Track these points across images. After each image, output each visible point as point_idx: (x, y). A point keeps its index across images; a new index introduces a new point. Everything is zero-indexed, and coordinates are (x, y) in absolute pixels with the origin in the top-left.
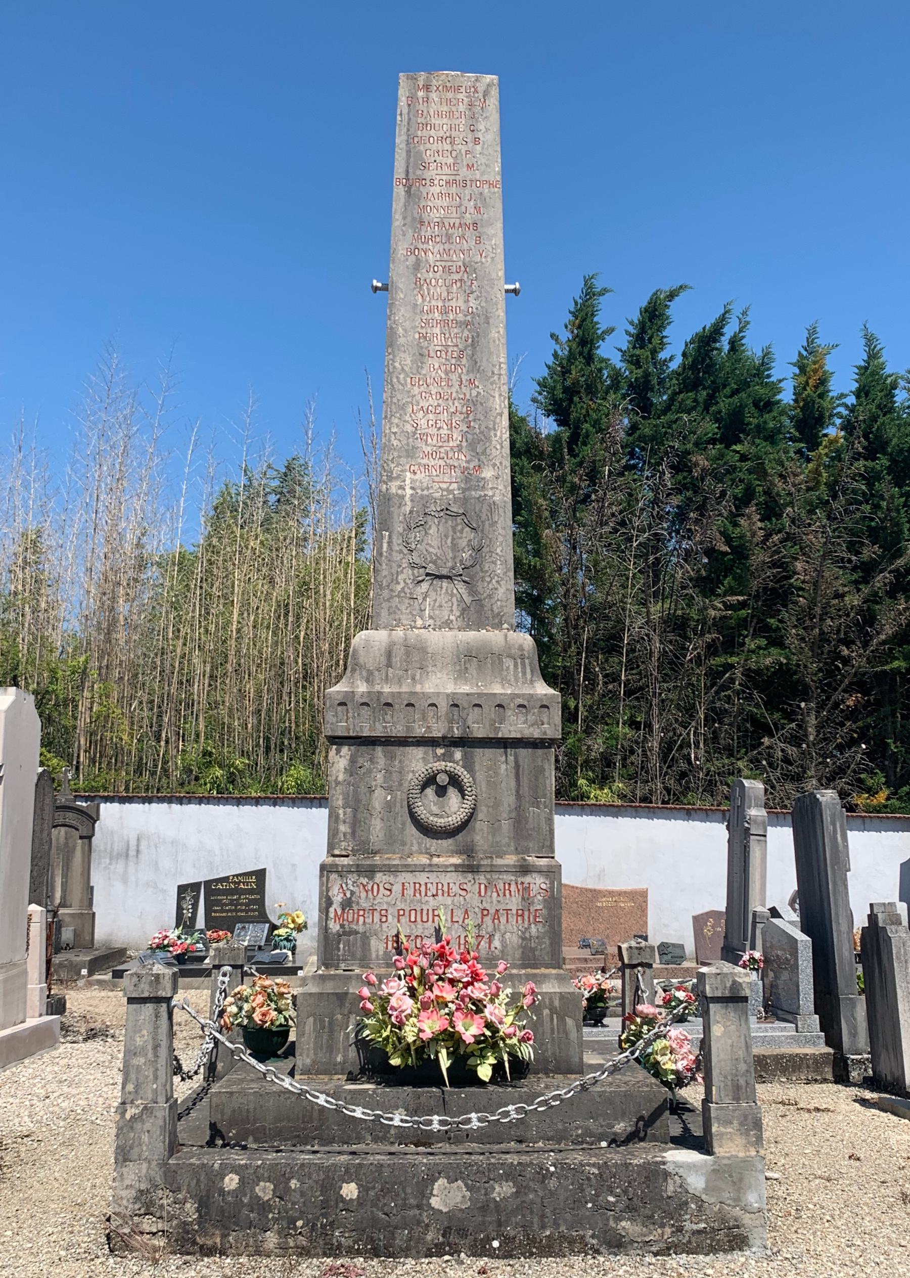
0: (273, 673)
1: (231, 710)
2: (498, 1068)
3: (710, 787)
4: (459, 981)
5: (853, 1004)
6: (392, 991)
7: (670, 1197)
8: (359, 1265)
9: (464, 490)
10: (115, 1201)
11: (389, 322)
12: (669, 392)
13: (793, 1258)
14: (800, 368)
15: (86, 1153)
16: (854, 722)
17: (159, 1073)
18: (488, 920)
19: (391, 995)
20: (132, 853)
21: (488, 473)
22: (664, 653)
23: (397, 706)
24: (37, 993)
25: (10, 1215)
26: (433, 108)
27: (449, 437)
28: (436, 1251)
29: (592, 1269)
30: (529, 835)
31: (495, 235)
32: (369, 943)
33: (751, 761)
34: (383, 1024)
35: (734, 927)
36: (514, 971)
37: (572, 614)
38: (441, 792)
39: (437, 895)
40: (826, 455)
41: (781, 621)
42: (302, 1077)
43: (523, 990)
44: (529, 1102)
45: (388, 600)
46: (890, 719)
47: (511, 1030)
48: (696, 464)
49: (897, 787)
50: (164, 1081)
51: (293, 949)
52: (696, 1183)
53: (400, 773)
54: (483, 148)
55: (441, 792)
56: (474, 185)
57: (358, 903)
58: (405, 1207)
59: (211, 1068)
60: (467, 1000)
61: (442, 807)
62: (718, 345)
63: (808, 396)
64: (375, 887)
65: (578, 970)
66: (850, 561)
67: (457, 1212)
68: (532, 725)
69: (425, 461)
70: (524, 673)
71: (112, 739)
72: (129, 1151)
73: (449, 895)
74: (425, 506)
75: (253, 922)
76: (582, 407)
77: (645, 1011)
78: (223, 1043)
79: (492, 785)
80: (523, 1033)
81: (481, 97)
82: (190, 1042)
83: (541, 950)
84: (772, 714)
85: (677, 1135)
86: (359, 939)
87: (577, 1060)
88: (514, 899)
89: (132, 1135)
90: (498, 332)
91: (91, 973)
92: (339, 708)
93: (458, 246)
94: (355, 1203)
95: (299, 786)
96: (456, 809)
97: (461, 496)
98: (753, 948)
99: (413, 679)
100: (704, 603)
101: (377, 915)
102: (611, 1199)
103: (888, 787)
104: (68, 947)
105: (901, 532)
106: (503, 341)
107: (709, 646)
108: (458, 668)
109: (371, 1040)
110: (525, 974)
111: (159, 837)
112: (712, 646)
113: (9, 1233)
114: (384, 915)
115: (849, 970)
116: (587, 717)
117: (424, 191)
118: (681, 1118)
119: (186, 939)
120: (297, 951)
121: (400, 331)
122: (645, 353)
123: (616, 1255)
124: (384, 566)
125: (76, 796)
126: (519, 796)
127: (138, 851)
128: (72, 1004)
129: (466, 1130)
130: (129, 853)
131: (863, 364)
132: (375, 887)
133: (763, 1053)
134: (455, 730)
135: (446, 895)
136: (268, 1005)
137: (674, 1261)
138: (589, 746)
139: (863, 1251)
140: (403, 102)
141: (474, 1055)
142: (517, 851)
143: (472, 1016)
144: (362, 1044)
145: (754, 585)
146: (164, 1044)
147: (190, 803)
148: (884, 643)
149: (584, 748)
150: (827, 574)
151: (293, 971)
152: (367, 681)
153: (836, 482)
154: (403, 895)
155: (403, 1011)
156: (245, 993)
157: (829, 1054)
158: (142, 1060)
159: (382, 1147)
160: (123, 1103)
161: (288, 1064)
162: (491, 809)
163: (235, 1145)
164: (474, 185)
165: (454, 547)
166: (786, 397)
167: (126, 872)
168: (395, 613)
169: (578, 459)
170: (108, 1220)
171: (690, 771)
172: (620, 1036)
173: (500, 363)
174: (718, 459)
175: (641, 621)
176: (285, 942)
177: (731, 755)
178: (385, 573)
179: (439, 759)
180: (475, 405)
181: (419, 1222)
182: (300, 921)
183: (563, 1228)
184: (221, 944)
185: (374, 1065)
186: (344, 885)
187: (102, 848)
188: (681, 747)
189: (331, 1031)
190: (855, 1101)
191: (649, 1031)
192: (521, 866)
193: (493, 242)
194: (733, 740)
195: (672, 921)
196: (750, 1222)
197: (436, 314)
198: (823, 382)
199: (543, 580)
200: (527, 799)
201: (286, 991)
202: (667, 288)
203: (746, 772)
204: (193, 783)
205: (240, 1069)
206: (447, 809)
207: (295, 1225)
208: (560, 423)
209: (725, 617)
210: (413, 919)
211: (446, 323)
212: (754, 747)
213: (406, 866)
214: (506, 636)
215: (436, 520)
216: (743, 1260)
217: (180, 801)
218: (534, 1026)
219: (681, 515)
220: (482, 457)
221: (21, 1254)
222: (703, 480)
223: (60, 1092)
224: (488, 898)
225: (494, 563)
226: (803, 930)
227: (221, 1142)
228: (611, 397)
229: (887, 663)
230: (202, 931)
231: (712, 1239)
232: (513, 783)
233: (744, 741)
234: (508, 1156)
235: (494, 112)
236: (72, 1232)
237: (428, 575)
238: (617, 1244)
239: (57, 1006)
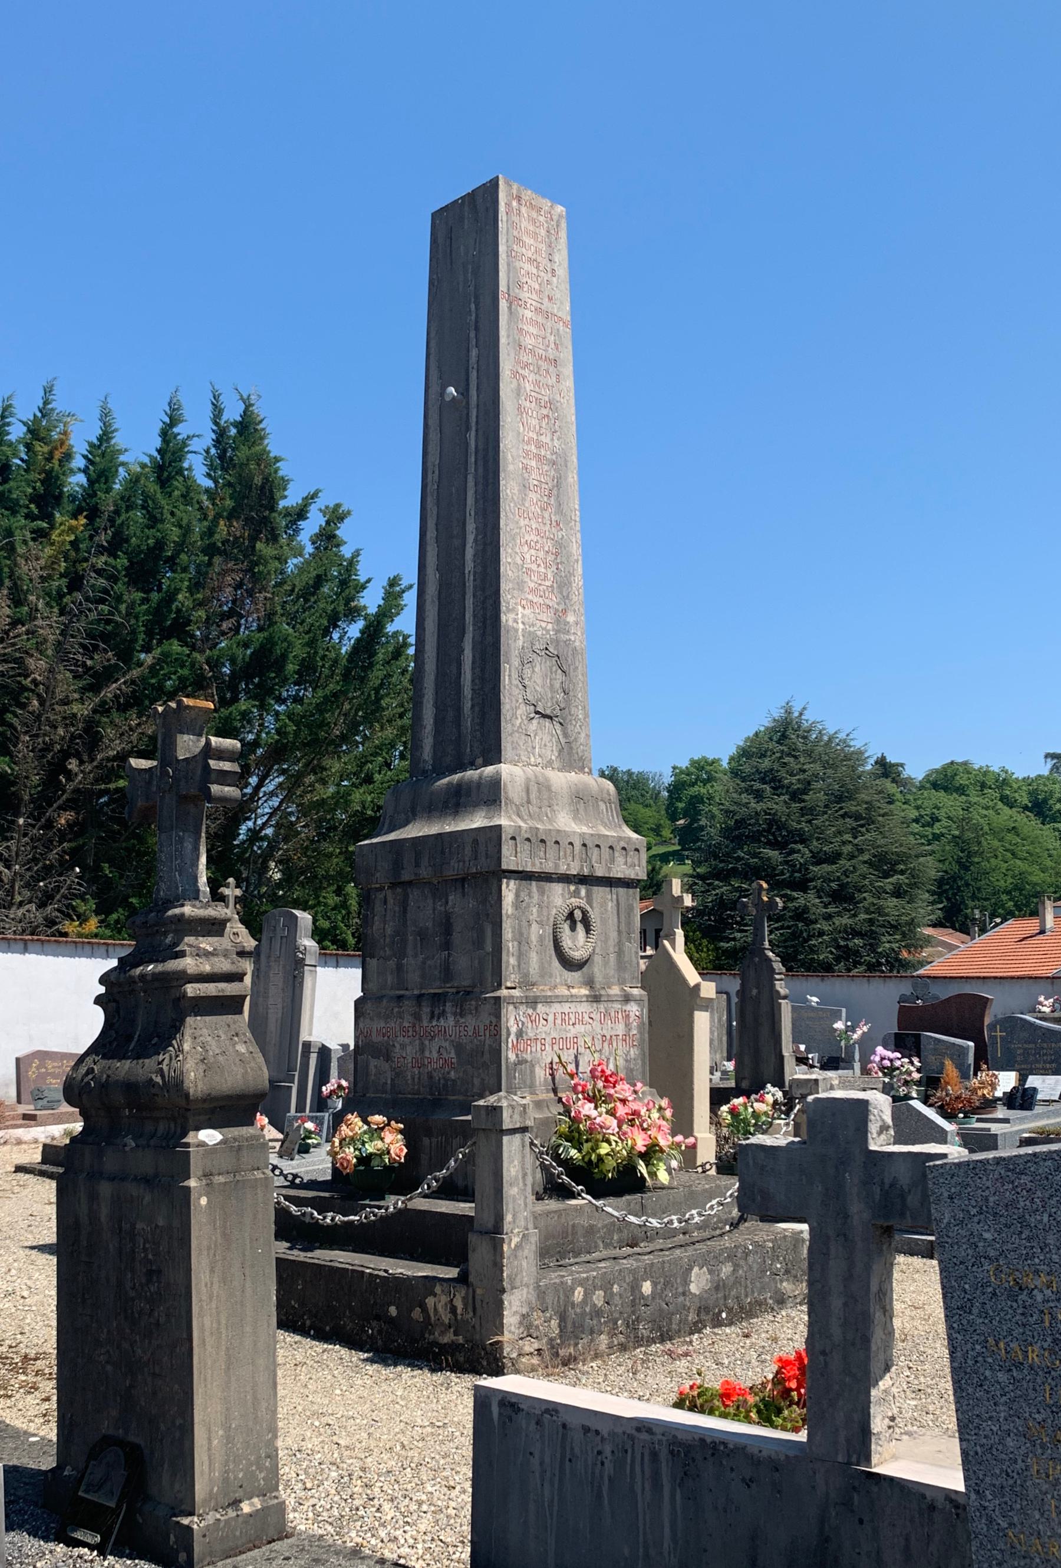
9: (557, 632)
45: (511, 735)
66: (84, 664)
69: (530, 597)
126: (619, 932)
225: (577, 707)
232: (616, 920)
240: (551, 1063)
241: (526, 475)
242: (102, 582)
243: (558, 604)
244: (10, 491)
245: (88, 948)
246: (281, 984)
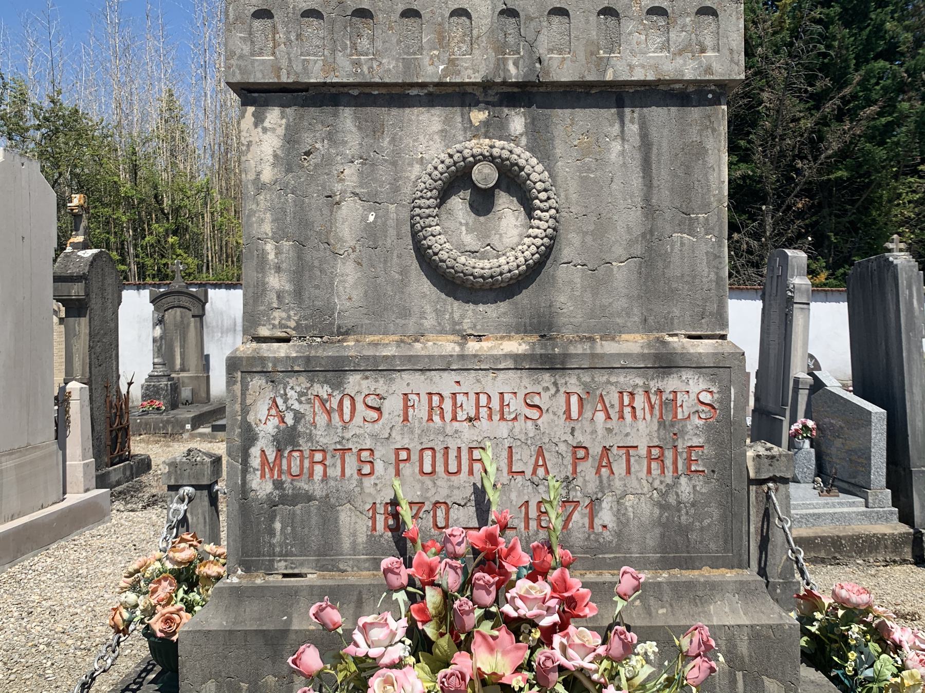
18: (587, 469)
23: (380, 17)
32: (336, 520)
38: (483, 203)
39: (477, 418)
53: (394, 164)
55: (483, 203)
57: (310, 438)
61: (484, 235)
64: (347, 403)
66: (806, 91)
68: (680, 53)
73: (502, 418)
83: (702, 529)
86: (314, 510)
88: (641, 425)
92: (257, 23)
96: (516, 240)
110: (669, 583)
114: (366, 459)
126: (650, 210)
132: (347, 403)
133: (837, 533)
135: (496, 417)
142: (645, 325)
150: (787, 102)
154: (406, 419)
157: (909, 534)
162: (589, 239)
179: (475, 132)
186: (280, 401)
187: (214, 324)
192: (657, 357)
200: (668, 215)
206: (495, 240)
210: (427, 468)
213: (410, 358)
224: (586, 424)
232: (636, 182)
242: (819, 28)
245: (822, 294)
246: (777, 321)
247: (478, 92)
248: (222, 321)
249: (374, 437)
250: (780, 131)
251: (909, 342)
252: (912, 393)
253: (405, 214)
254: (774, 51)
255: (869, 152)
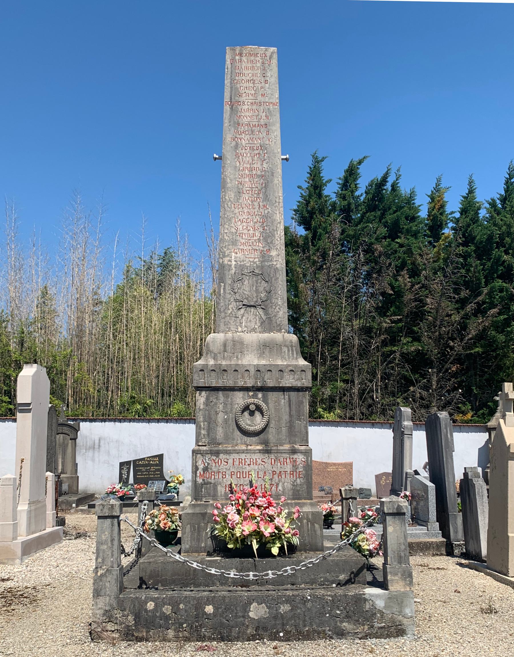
0: (164, 357)
1: (144, 376)
2: (281, 549)
3: (383, 412)
4: (262, 506)
5: (455, 517)
6: (228, 512)
7: (367, 611)
8: (214, 645)
9: (262, 262)
10: (93, 616)
11: (222, 176)
12: (361, 212)
13: (428, 640)
14: (431, 199)
15: (78, 593)
16: (456, 379)
17: (114, 553)
18: (276, 476)
19: (228, 513)
20: (96, 446)
21: (274, 253)
22: (360, 346)
23: (229, 371)
24: (51, 515)
25: (41, 623)
26: (244, 65)
27: (254, 235)
28: (252, 638)
29: (329, 646)
30: (296, 435)
31: (276, 130)
33: (404, 399)
34: (225, 528)
35: (397, 479)
36: (289, 501)
37: (315, 326)
38: (252, 414)
40: (443, 244)
41: (420, 329)
42: (185, 554)
43: (294, 510)
44: (297, 565)
45: (224, 318)
46: (474, 377)
47: (288, 530)
48: (376, 250)
49: (477, 410)
50: (116, 557)
51: (178, 493)
52: (380, 604)
54: (269, 85)
55: (252, 414)
56: (265, 104)
57: (211, 469)
58: (236, 616)
59: (139, 552)
60: (266, 515)
61: (252, 421)
62: (385, 187)
63: (435, 214)
64: (220, 461)
65: (319, 502)
66: (454, 298)
67: (262, 619)
69: (242, 247)
70: (293, 354)
71: (84, 390)
72: (100, 591)
74: (242, 270)
75: (157, 480)
76: (318, 221)
77: (354, 520)
78: (145, 538)
79: (277, 410)
80: (294, 531)
81: (268, 59)
82: (128, 539)
84: (415, 375)
85: (370, 581)
87: (320, 544)
88: (288, 466)
89: (101, 583)
90: (278, 180)
91: (77, 506)
92: (200, 372)
93: (258, 136)
94: (212, 615)
95: (179, 413)
97: (260, 265)
98: (406, 490)
99: (237, 357)
100: (381, 320)
101: (220, 475)
102: (338, 612)
103: (473, 411)
104: (66, 493)
105: (481, 283)
106: (281, 185)
107: (383, 341)
108: (260, 352)
109: (219, 536)
111: (110, 439)
112: (385, 341)
113: (41, 631)
114: (224, 475)
115: (454, 501)
116: (322, 378)
117: (240, 108)
118: (372, 573)
119: (124, 489)
120: (179, 494)
121: (228, 180)
122: (348, 193)
123: (341, 639)
124: (222, 301)
125: (68, 419)
126: (291, 416)
127: (99, 446)
128: (68, 521)
129: (266, 579)
130: (95, 447)
131: (465, 195)
132: (220, 461)
134: (259, 384)
136: (167, 519)
137: (370, 642)
138: (323, 392)
139: (462, 636)
140: (228, 62)
141: (270, 543)
142: (290, 443)
143: (269, 523)
144: (214, 538)
145: (406, 310)
146: (116, 539)
147: (125, 422)
148: (471, 339)
149: (321, 393)
150: (443, 305)
151: (178, 504)
152: (214, 359)
153: (448, 258)
155: (234, 521)
156: (156, 514)
157: (444, 542)
158: (105, 547)
159: (225, 588)
160: (96, 568)
161: (178, 547)
163: (152, 588)
164: (265, 104)
165: (257, 291)
166: (423, 214)
167: (93, 456)
168: (227, 324)
169: (316, 248)
170: (90, 625)
171: (374, 404)
172: (341, 533)
173: (279, 196)
174: (388, 247)
175: (349, 329)
176: (173, 490)
177: (394, 396)
178: (222, 304)
179: (250, 397)
180: (267, 218)
181: (243, 624)
182: (181, 479)
183: (314, 626)
184: (143, 490)
185: (220, 548)
187: (81, 444)
188: (369, 393)
189: (199, 531)
190: (457, 564)
191: (356, 530)
192: (292, 450)
193: (275, 134)
194: (395, 388)
195: (364, 478)
196: (406, 623)
197: (247, 171)
198: (442, 206)
199: (300, 309)
200: (295, 417)
201: (176, 512)
202: (356, 160)
203: (401, 404)
204: (126, 412)
205: (154, 551)
206: (255, 422)
207: (182, 626)
208: (306, 229)
209: (391, 327)
210: (238, 476)
211: (251, 176)
212: (405, 392)
213: (234, 450)
214: (283, 336)
215: (248, 278)
216: (403, 641)
217: (120, 421)
218: (299, 528)
219: (369, 275)
220: (271, 245)
221: (48, 641)
222: (380, 257)
223: (64, 564)
226: (431, 481)
227: (145, 586)
228: (332, 215)
229: (473, 349)
230: (132, 485)
231: (388, 631)
232: (287, 409)
233: (400, 389)
234: (287, 592)
235: (275, 67)
236: (72, 631)
237: (244, 305)
238: (341, 634)
239: (61, 522)
240: (231, 485)
241: (241, 187)
243: (263, 247)
244: (411, 228)
247: (251, 388)
248: (86, 442)
249: (226, 469)
250: (438, 323)
251: (446, 454)
252: (448, 477)
253: (234, 416)
254: (434, 273)
255: (494, 337)
